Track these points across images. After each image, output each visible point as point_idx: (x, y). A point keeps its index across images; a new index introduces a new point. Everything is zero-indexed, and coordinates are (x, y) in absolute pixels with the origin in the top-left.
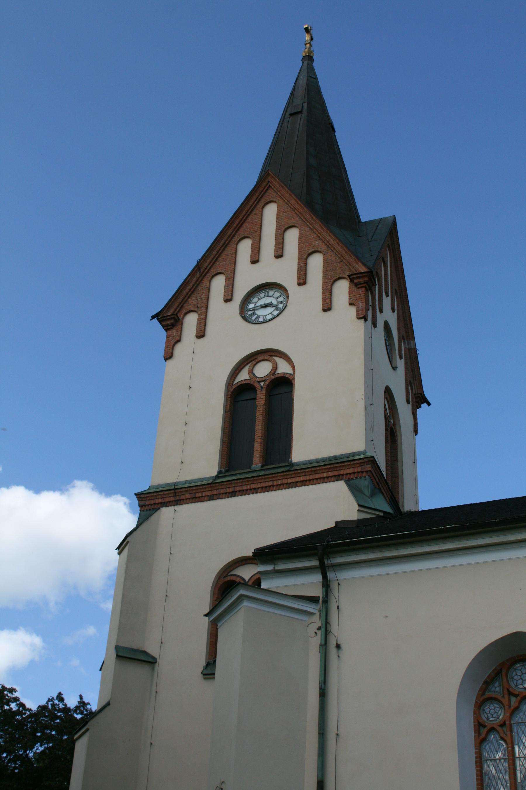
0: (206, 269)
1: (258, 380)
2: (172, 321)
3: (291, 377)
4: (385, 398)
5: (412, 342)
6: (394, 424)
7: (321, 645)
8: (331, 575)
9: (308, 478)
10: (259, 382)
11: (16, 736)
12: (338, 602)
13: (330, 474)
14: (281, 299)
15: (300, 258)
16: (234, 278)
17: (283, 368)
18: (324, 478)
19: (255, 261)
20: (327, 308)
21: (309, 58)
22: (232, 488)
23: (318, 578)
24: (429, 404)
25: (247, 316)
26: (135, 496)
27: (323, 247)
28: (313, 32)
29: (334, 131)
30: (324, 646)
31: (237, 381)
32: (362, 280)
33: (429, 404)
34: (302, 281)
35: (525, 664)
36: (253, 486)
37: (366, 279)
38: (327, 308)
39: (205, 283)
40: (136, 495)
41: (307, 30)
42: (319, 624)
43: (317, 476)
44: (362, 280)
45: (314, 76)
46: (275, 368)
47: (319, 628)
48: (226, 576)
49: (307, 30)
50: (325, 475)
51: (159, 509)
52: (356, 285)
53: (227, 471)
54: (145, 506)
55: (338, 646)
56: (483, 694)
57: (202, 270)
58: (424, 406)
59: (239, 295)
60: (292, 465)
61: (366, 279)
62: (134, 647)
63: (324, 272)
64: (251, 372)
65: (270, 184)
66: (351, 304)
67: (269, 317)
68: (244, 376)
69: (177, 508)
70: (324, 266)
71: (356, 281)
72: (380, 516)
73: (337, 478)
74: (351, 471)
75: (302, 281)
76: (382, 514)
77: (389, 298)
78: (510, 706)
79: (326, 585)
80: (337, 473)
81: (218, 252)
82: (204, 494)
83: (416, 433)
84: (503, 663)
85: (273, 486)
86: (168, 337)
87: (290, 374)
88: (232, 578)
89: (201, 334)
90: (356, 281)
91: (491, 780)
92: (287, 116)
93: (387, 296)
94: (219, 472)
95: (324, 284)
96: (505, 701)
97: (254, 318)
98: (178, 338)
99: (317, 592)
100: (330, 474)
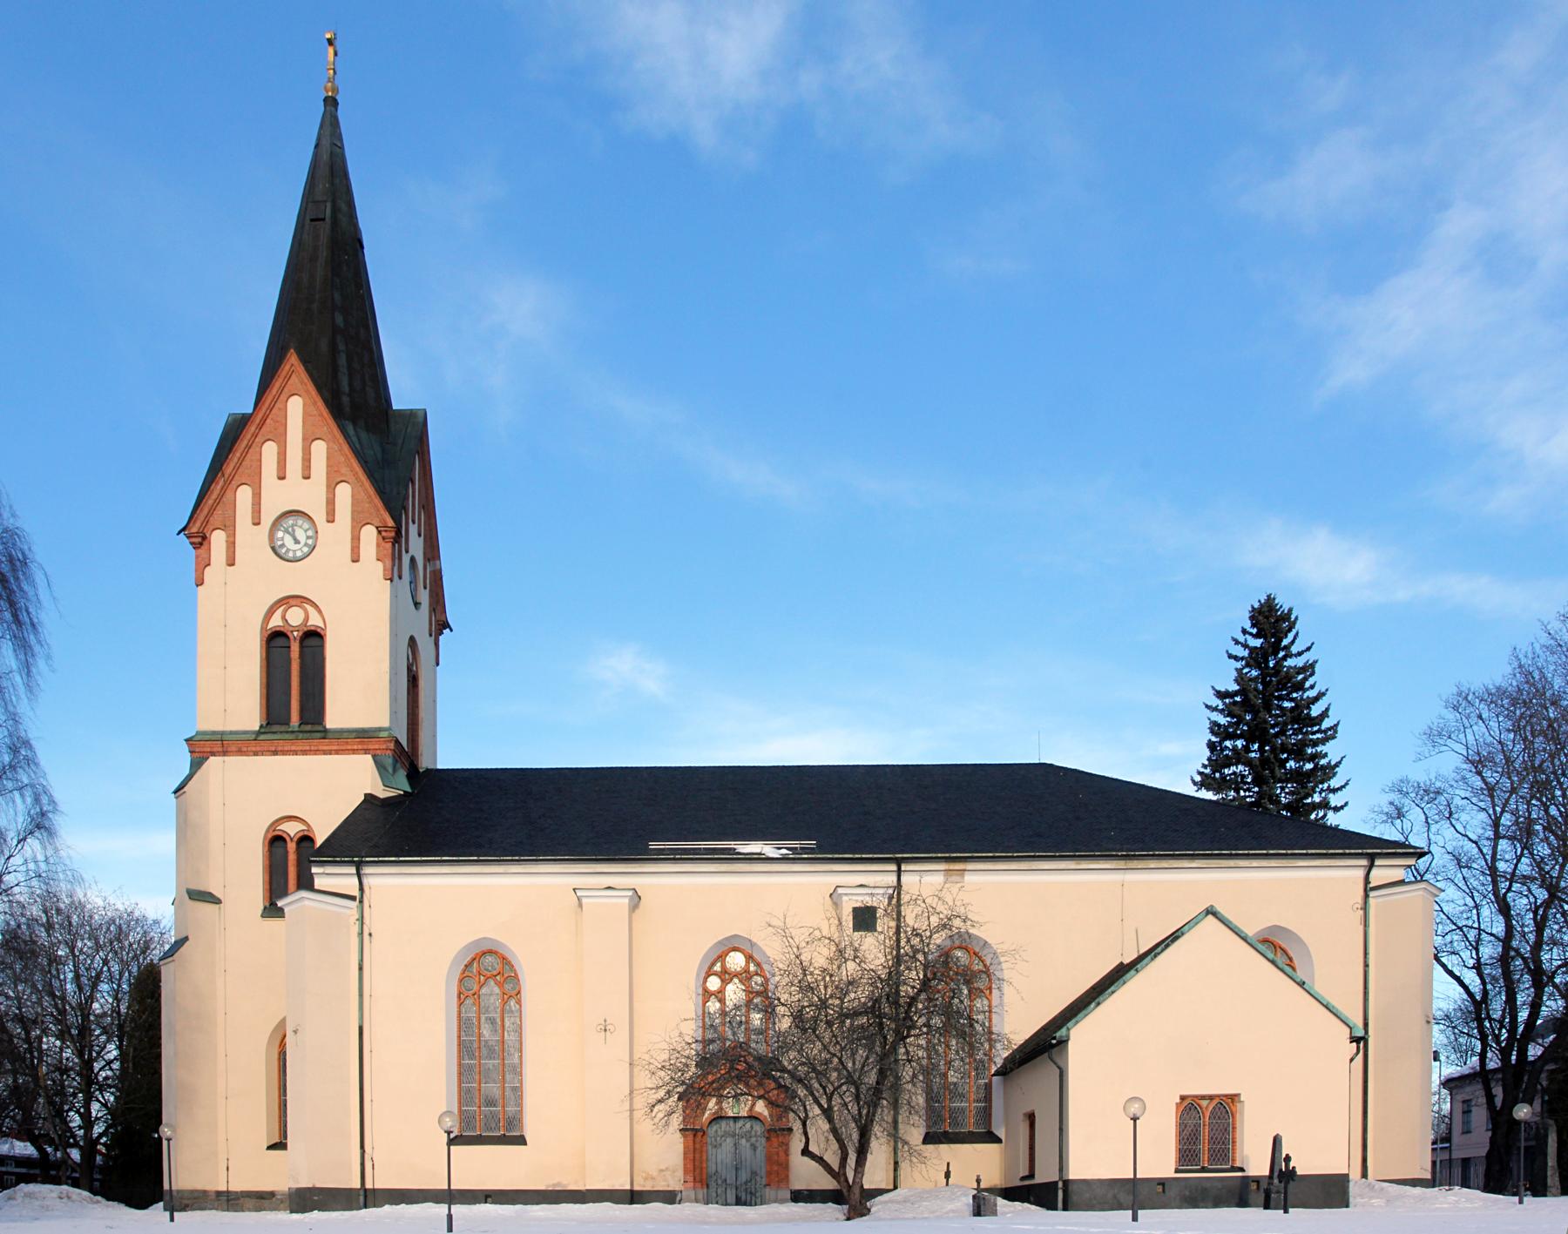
0: (230, 475)
1: (291, 629)
2: (199, 540)
3: (322, 633)
4: (409, 645)
5: (438, 562)
6: (417, 671)
7: (359, 934)
9: (342, 748)
10: (292, 632)
11: (315, 1196)
12: (369, 902)
13: (360, 747)
14: (310, 533)
15: (328, 486)
16: (260, 494)
17: (315, 621)
18: (354, 750)
20: (355, 560)
21: (331, 102)
24: (451, 630)
25: (277, 548)
26: (185, 742)
27: (352, 479)
28: (337, 43)
29: (362, 247)
31: (270, 626)
33: (451, 630)
36: (293, 748)
38: (355, 560)
39: (229, 494)
40: (187, 740)
41: (330, 42)
42: (357, 917)
43: (349, 747)
45: (339, 145)
46: (307, 618)
47: (357, 920)
48: (274, 831)
49: (330, 42)
50: (355, 747)
51: (208, 758)
52: (384, 538)
53: (268, 724)
54: (195, 752)
55: (370, 935)
56: (464, 973)
57: (226, 476)
58: (446, 631)
59: (267, 519)
60: (326, 731)
62: (202, 889)
63: (353, 512)
64: (284, 618)
65: (293, 368)
66: (378, 560)
67: (299, 554)
68: (276, 622)
69: (226, 758)
70: (353, 505)
71: (384, 534)
72: (400, 795)
73: (366, 751)
74: (377, 747)
76: (402, 793)
77: (416, 525)
78: (479, 982)
80: (365, 747)
81: (241, 455)
82: (249, 749)
83: (438, 664)
84: (477, 954)
85: (311, 750)
86: (197, 557)
87: (322, 629)
88: (280, 833)
89: (231, 562)
90: (384, 534)
92: (308, 221)
93: (414, 522)
94: (261, 726)
95: (353, 527)
97: (284, 551)
98: (207, 563)
100: (360, 747)
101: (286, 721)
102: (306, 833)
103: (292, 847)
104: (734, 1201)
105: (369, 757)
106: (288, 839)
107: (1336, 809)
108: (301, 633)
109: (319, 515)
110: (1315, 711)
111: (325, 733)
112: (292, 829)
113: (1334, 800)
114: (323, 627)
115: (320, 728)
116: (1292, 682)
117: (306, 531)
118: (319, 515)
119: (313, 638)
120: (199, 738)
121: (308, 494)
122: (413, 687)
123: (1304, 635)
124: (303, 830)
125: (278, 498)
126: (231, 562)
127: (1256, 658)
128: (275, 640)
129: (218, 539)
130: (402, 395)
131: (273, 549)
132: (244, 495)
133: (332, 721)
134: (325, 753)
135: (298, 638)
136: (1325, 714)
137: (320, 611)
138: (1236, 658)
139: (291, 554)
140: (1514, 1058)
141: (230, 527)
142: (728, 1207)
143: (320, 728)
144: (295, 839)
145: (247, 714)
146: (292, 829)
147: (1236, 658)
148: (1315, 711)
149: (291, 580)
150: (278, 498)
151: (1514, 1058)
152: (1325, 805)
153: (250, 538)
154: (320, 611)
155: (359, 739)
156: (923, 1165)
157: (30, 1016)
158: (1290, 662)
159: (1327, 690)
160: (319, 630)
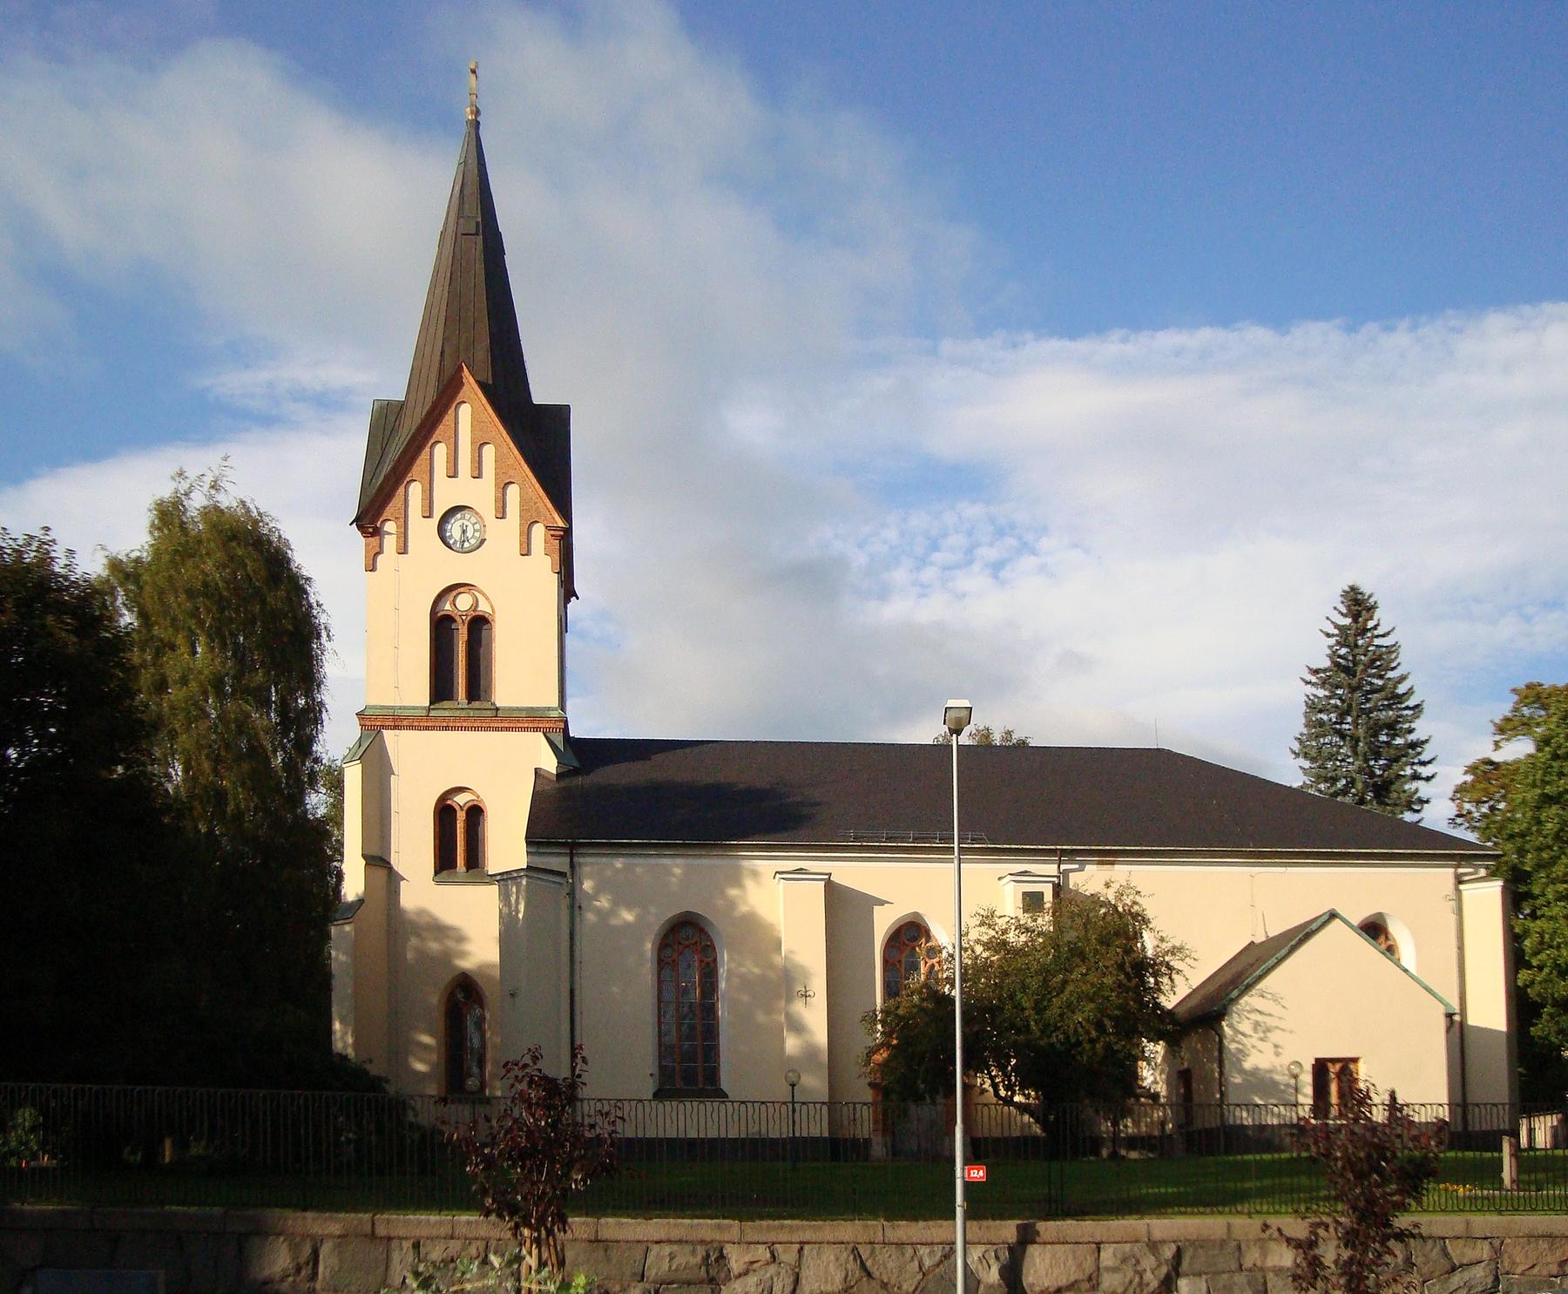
8: (576, 859)
17: (484, 607)
19: (453, 474)
20: (526, 552)
22: (1129, 1245)
23: (567, 860)
24: (578, 598)
30: (572, 907)
32: (558, 533)
33: (578, 598)
34: (502, 514)
35: (800, 988)
37: (562, 533)
38: (526, 552)
41: (474, 72)
44: (558, 533)
55: (580, 907)
61: (562, 533)
73: (536, 729)
75: (502, 514)
79: (572, 866)
89: (403, 550)
91: (530, 1106)
96: (676, 947)
99: (566, 869)
102: (475, 803)
106: (457, 808)
107: (1428, 779)
108: (469, 618)
110: (1401, 689)
113: (1425, 771)
114: (491, 612)
115: (488, 705)
116: (1382, 660)
117: (474, 525)
119: (479, 624)
121: (478, 493)
122: (1260, 960)
123: (1383, 618)
124: (473, 800)
125: (447, 494)
127: (1346, 637)
128: (441, 626)
130: (541, 394)
134: (497, 729)
135: (466, 622)
136: (1410, 692)
137: (487, 598)
138: (1328, 635)
140: (28, 700)
143: (488, 705)
144: (465, 809)
145: (417, 693)
147: (1328, 635)
148: (1401, 689)
149: (454, 568)
151: (28, 700)
152: (1416, 777)
153: (422, 530)
154: (487, 598)
155: (528, 719)
156: (1187, 959)
158: (1377, 642)
159: (1409, 673)
160: (487, 616)
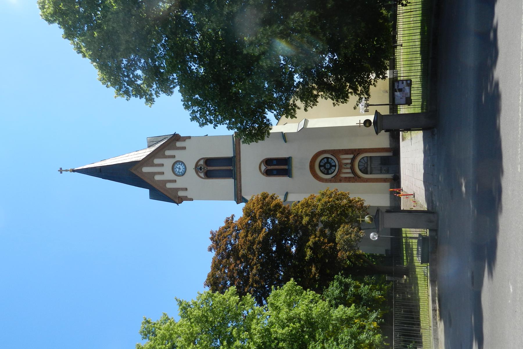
59: (173, 177)
94: (233, 179)
97: (183, 172)
101: (231, 171)
103: (269, 167)
104: (370, 174)
105: (232, 155)
109: (173, 161)
111: (234, 157)
112: (263, 168)
118: (173, 161)
120: (236, 200)
126: (186, 189)
129: (181, 194)
131: (183, 175)
132: (169, 186)
133: (230, 154)
139: (184, 170)
140: (464, 189)
141: (177, 190)
142: (376, 211)
146: (263, 168)
150: (169, 175)
151: (464, 189)
153: (180, 182)
157: (320, 264)
